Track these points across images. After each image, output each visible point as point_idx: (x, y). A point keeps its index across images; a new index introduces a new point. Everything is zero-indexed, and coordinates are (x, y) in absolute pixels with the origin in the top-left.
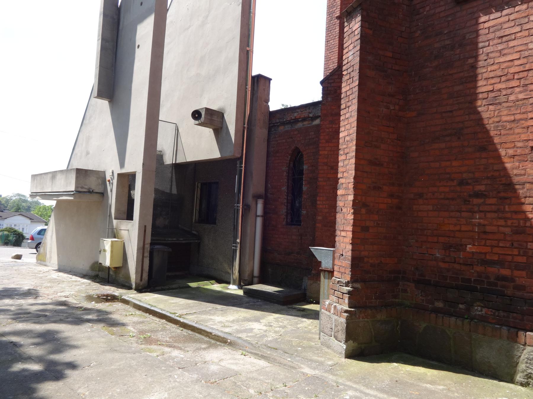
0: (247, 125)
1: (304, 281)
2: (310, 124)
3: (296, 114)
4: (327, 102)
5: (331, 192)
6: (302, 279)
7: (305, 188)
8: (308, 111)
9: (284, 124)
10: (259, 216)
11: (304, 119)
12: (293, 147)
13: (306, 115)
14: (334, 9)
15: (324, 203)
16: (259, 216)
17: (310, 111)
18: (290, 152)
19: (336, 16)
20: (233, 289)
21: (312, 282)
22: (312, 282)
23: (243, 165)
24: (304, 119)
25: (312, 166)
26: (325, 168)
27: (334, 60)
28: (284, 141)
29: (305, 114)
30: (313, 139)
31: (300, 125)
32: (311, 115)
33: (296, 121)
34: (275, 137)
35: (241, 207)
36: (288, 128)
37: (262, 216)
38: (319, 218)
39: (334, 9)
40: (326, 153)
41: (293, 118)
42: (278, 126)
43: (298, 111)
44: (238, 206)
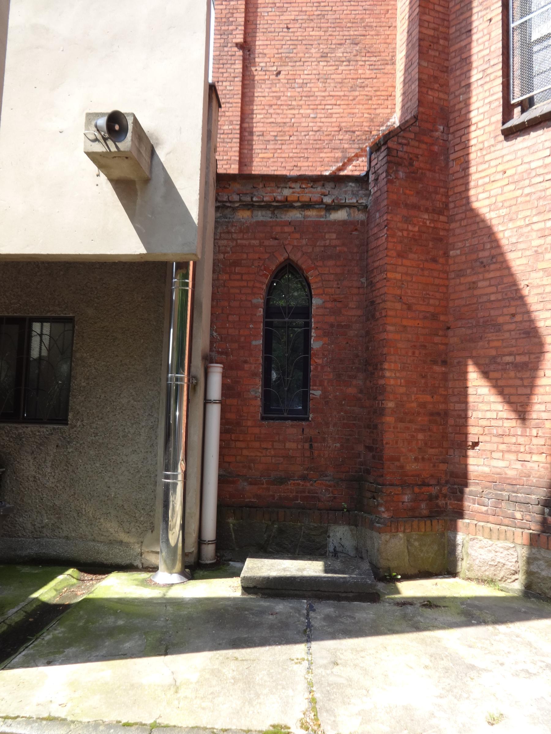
0: (228, 190)
1: (331, 534)
2: (321, 216)
3: (287, 192)
4: (396, 178)
5: (410, 354)
6: (326, 532)
7: (316, 344)
8: (319, 189)
9: (251, 206)
10: (215, 402)
11: (307, 206)
12: (282, 259)
13: (316, 197)
14: (231, 28)
15: (398, 375)
16: (215, 402)
17: (326, 191)
18: (273, 267)
19: (234, 41)
20: (167, 584)
21: (388, 537)
22: (388, 537)
23: (190, 281)
24: (307, 206)
25: (335, 300)
26: (398, 306)
27: (231, 118)
28: (256, 242)
29: (313, 194)
30: (335, 247)
31: (295, 215)
32: (327, 200)
33: (287, 205)
34: (229, 232)
35: (186, 380)
36: (261, 216)
37: (221, 402)
38: (391, 405)
39: (231, 28)
40: (398, 276)
41: (279, 198)
42: (234, 209)
43: (293, 185)
44: (177, 379)
